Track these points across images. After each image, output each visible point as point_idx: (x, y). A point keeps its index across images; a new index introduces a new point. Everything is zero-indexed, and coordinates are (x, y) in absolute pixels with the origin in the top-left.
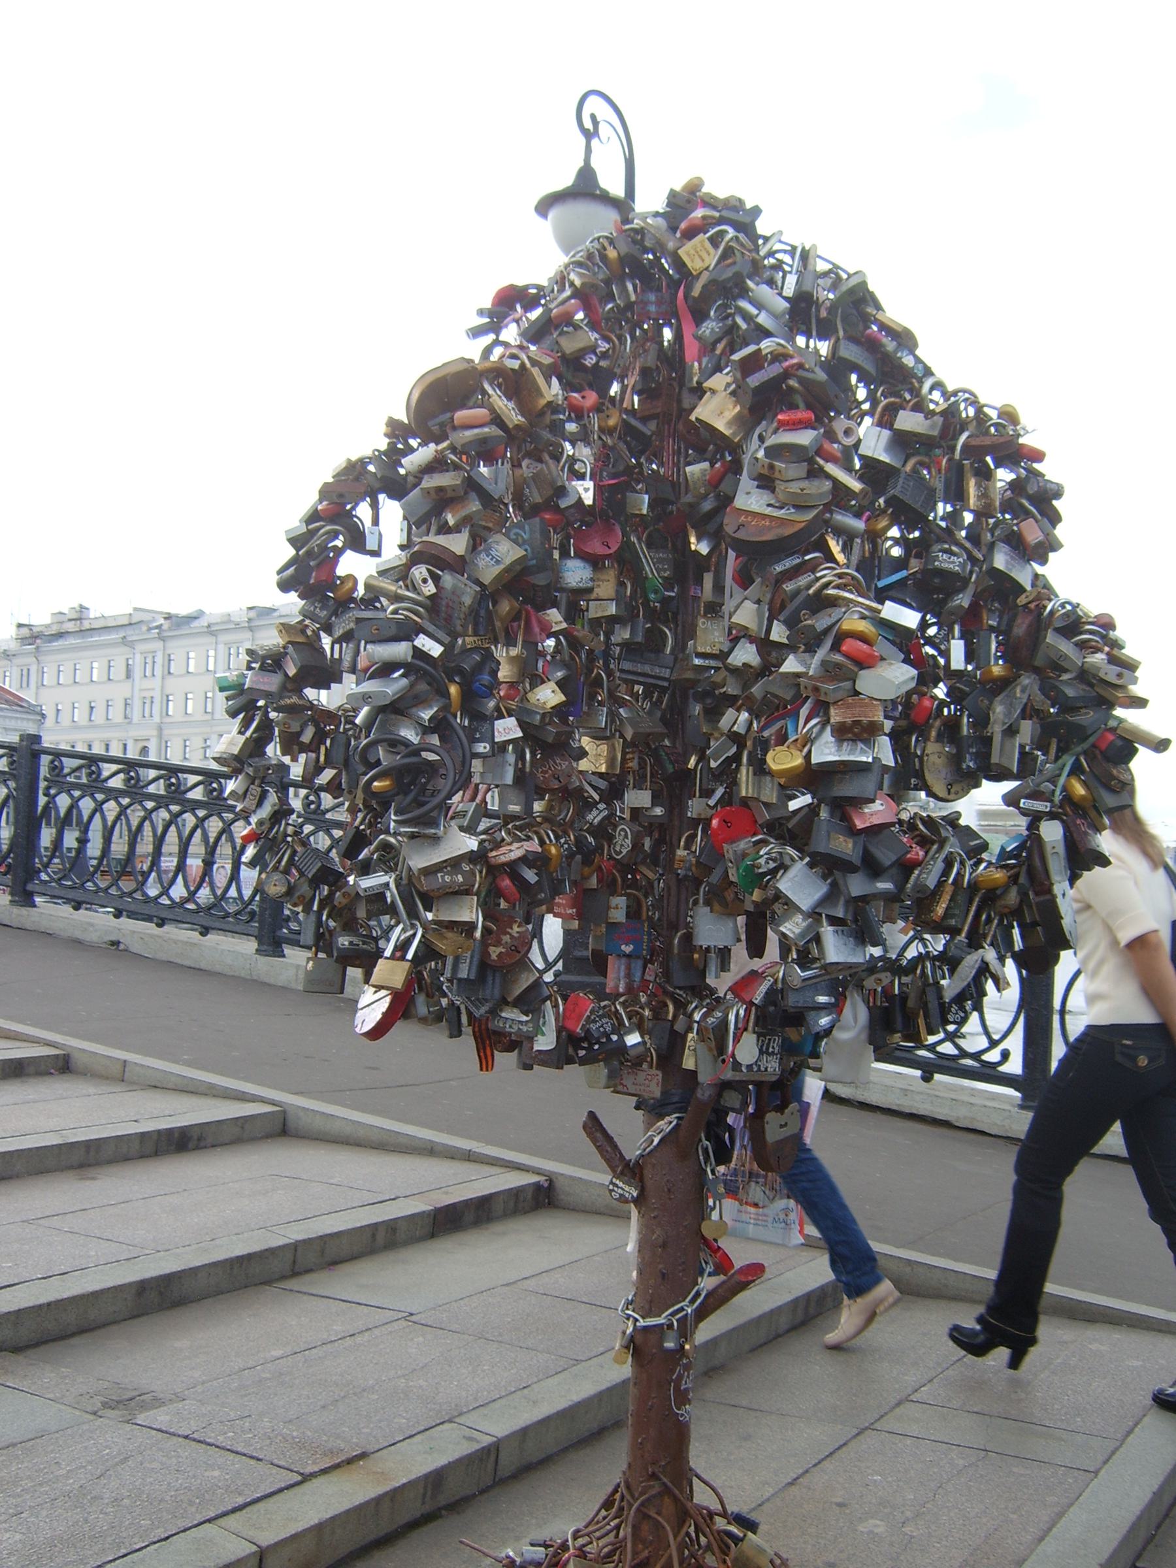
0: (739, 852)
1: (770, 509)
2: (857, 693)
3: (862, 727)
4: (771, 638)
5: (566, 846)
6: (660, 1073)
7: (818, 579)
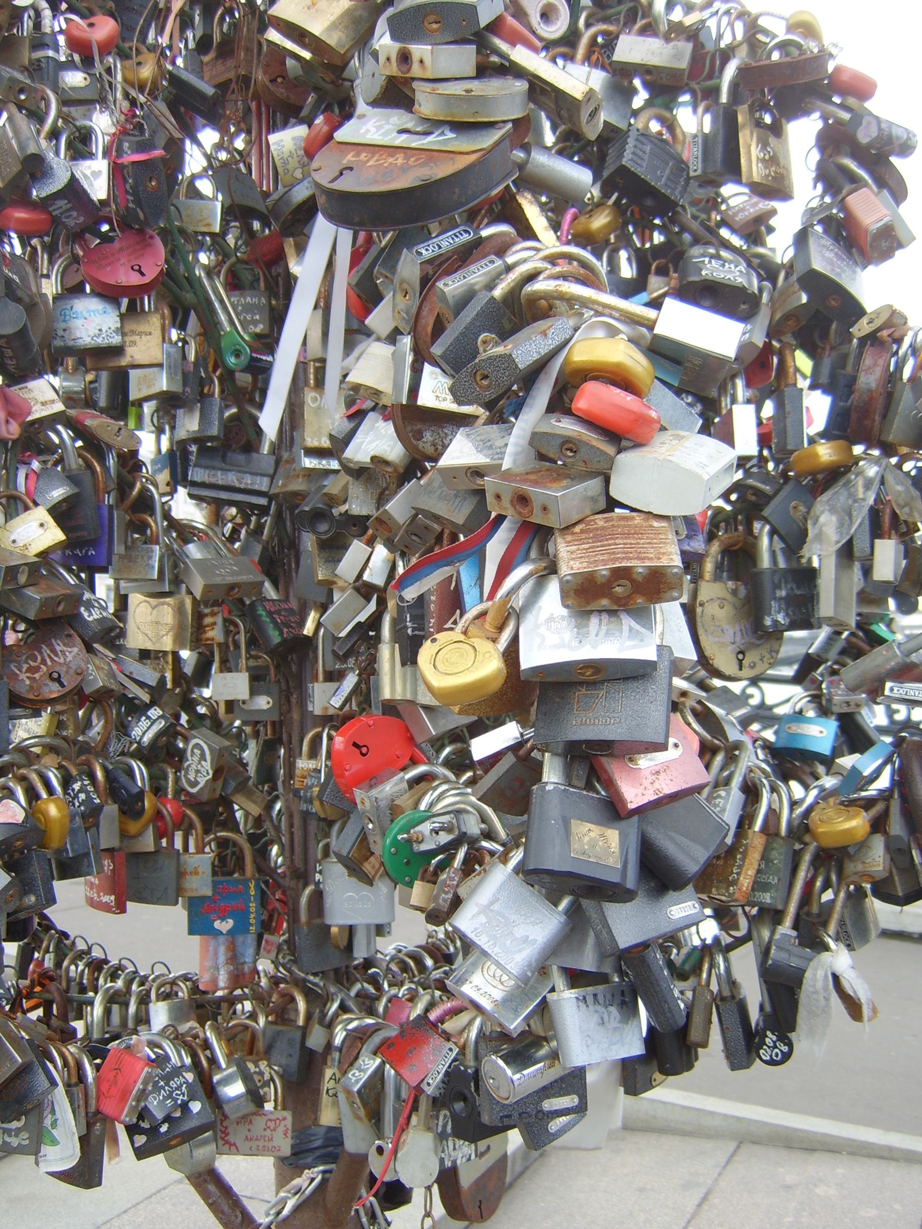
0: (383, 804)
1: (404, 136)
2: (612, 504)
3: (633, 581)
4: (419, 403)
5: (82, 796)
6: (288, 1115)
7: (509, 269)
